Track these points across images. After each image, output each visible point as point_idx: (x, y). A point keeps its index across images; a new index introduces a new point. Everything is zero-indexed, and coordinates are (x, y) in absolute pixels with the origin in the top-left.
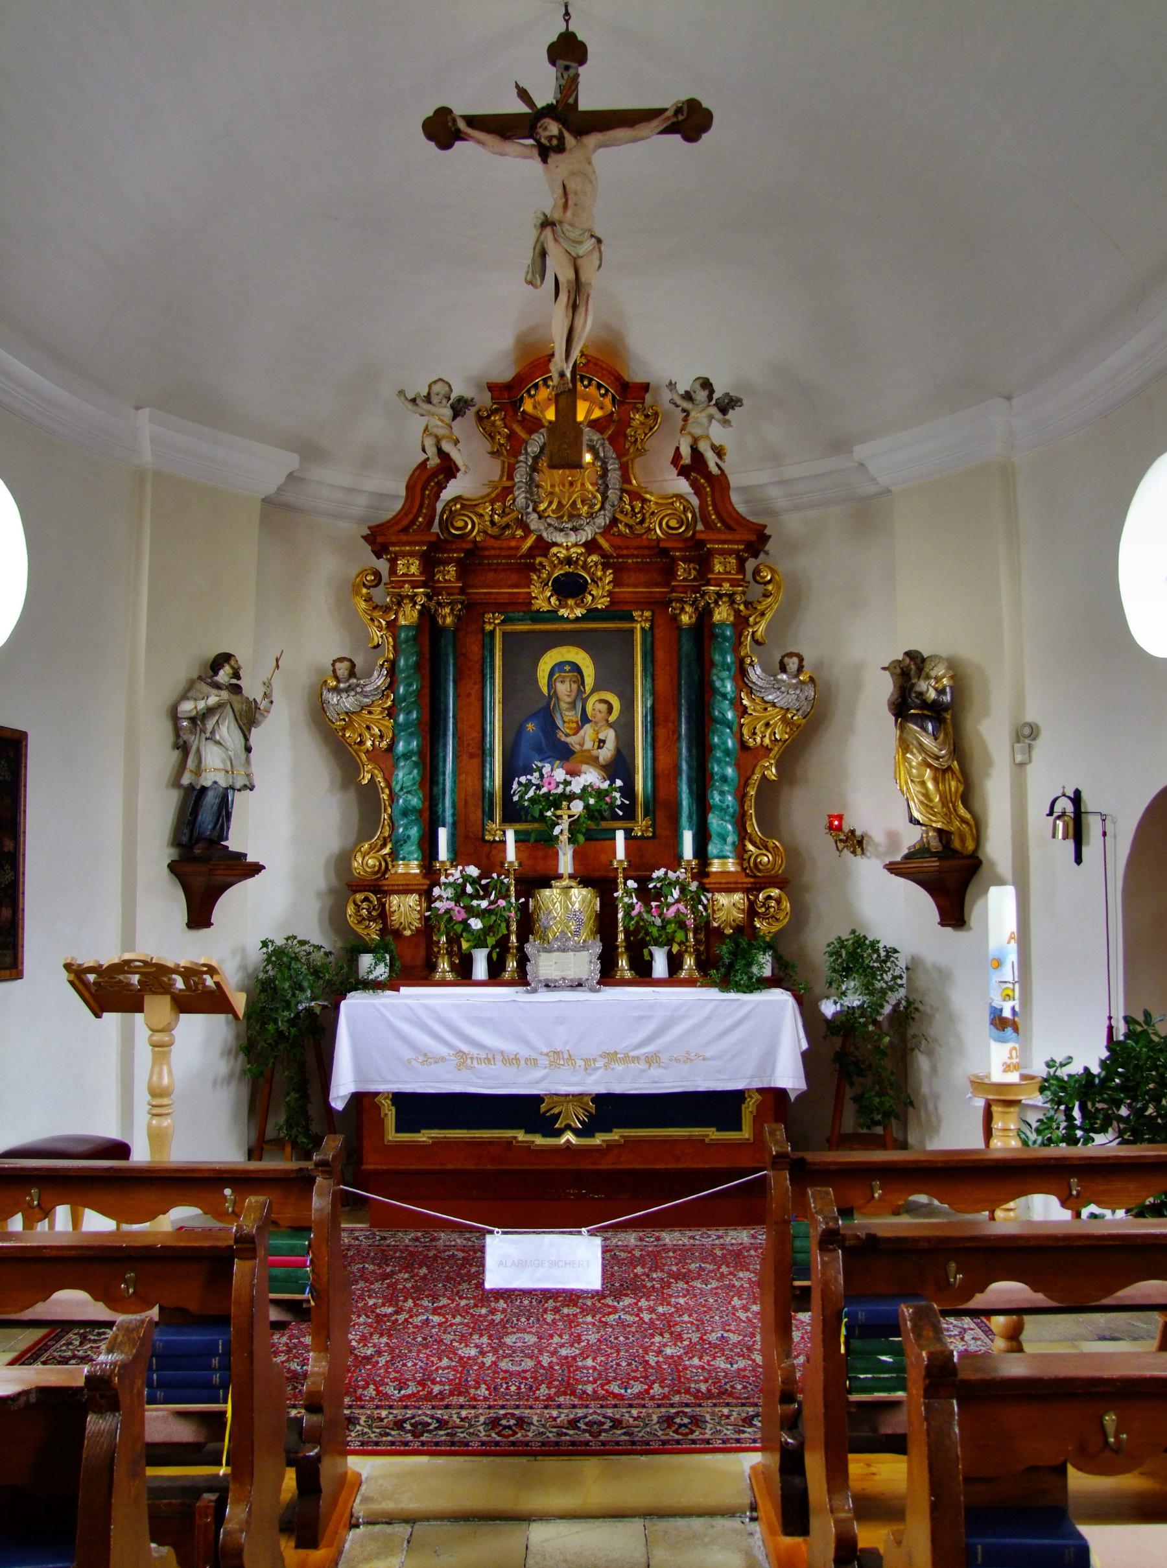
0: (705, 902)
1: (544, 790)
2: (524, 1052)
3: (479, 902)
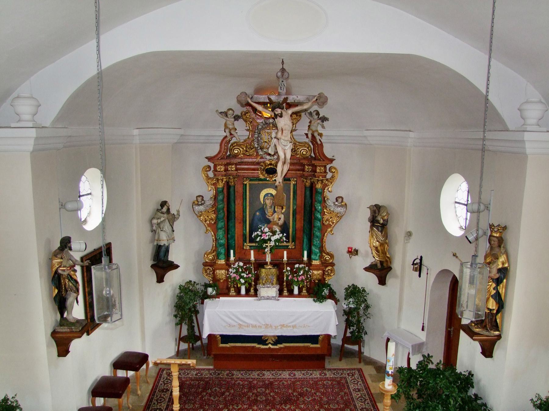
2: (258, 324)
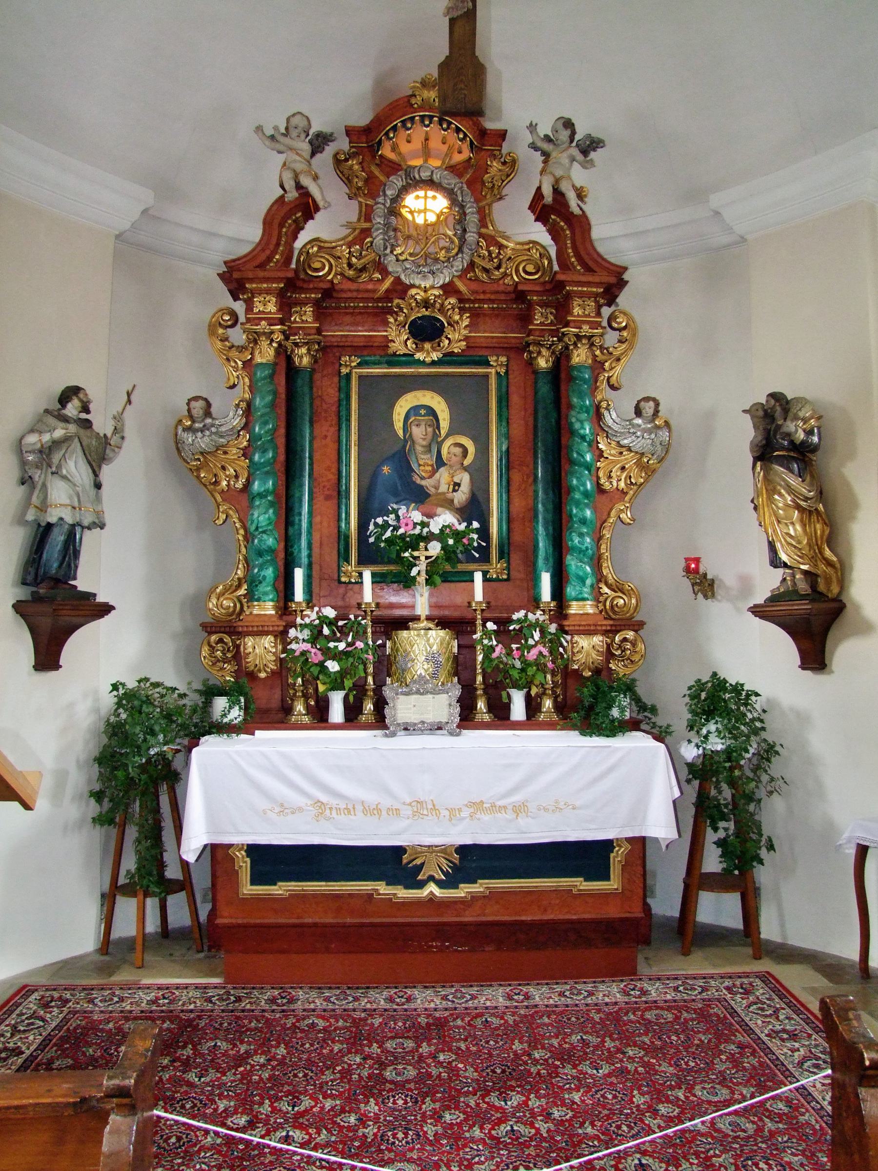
0: (565, 644)
1: (401, 531)
2: (386, 802)
3: (336, 644)
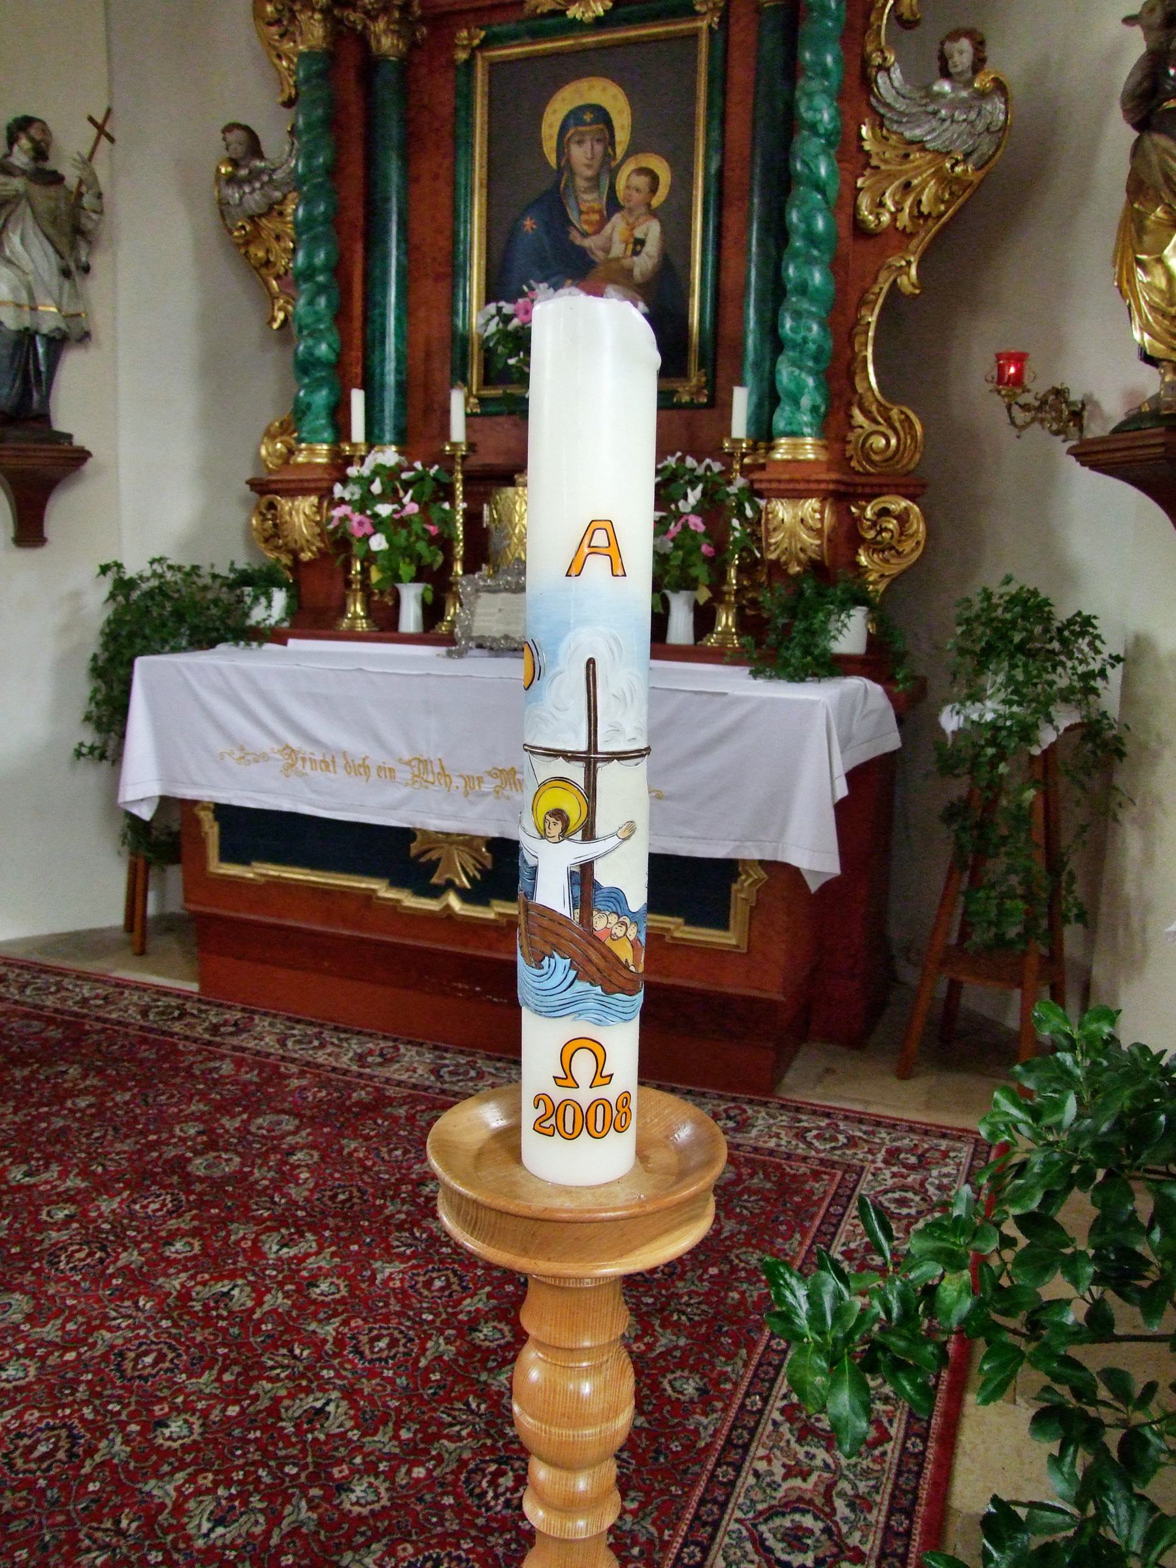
2: (377, 757)
